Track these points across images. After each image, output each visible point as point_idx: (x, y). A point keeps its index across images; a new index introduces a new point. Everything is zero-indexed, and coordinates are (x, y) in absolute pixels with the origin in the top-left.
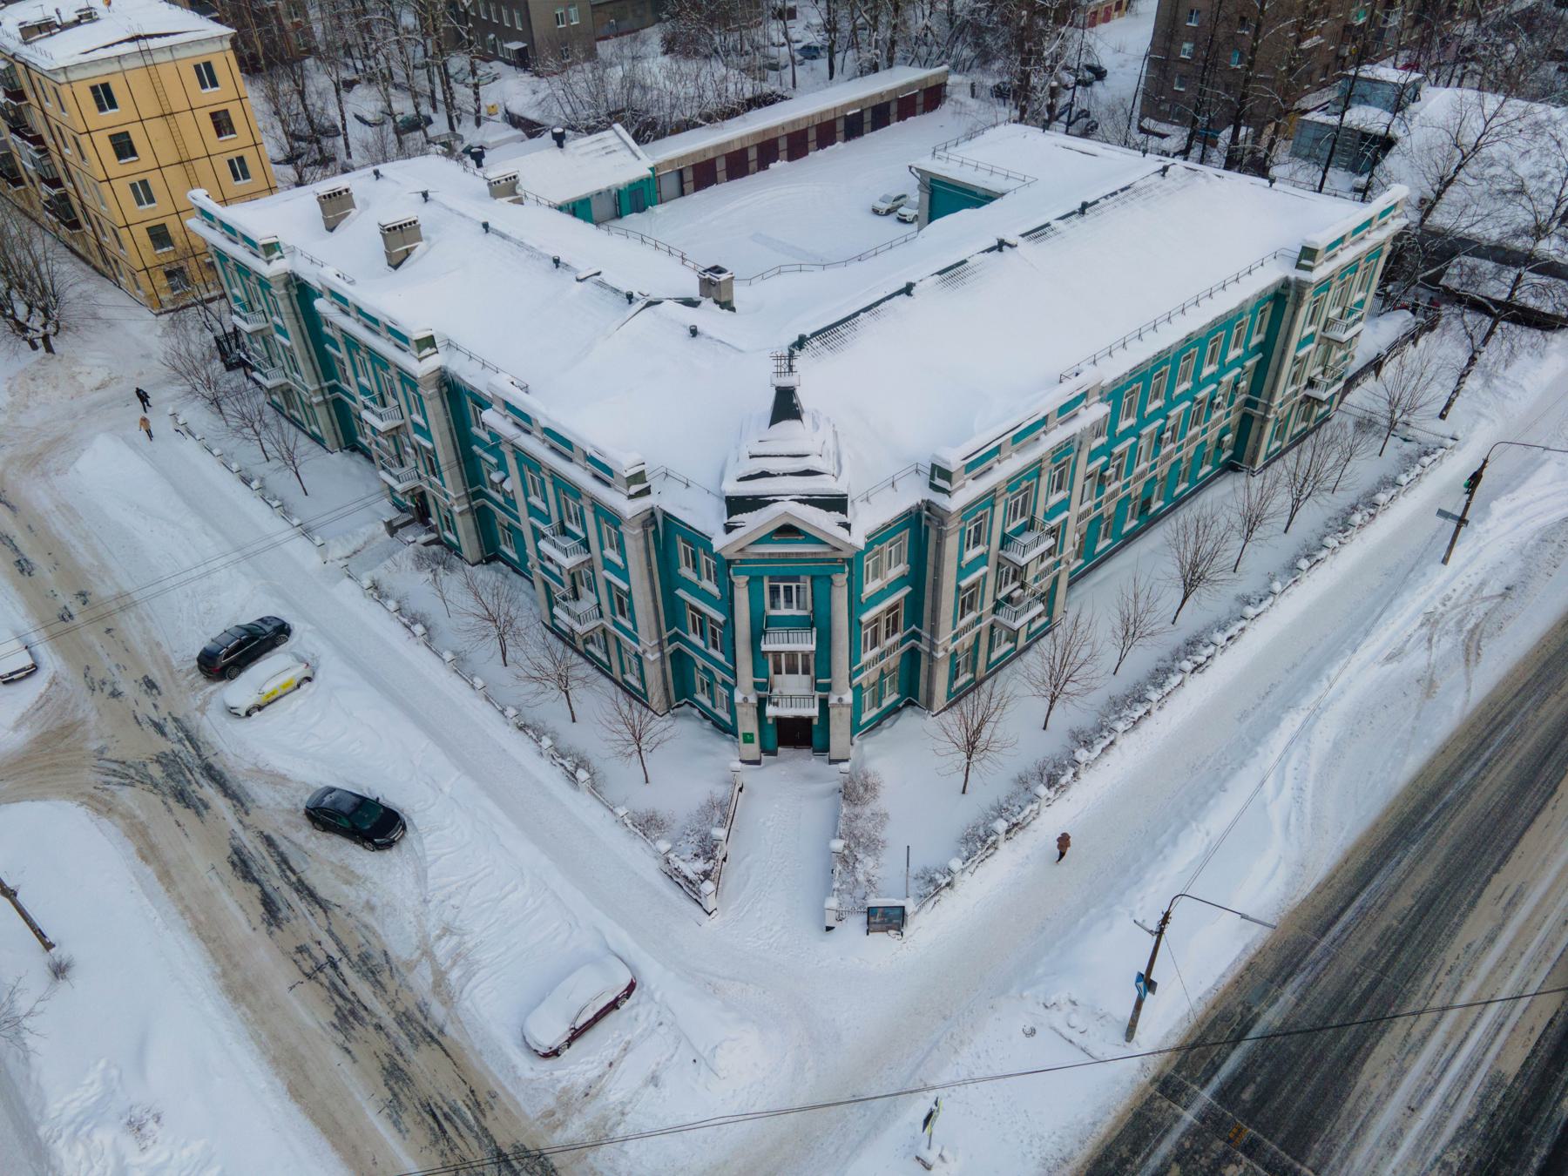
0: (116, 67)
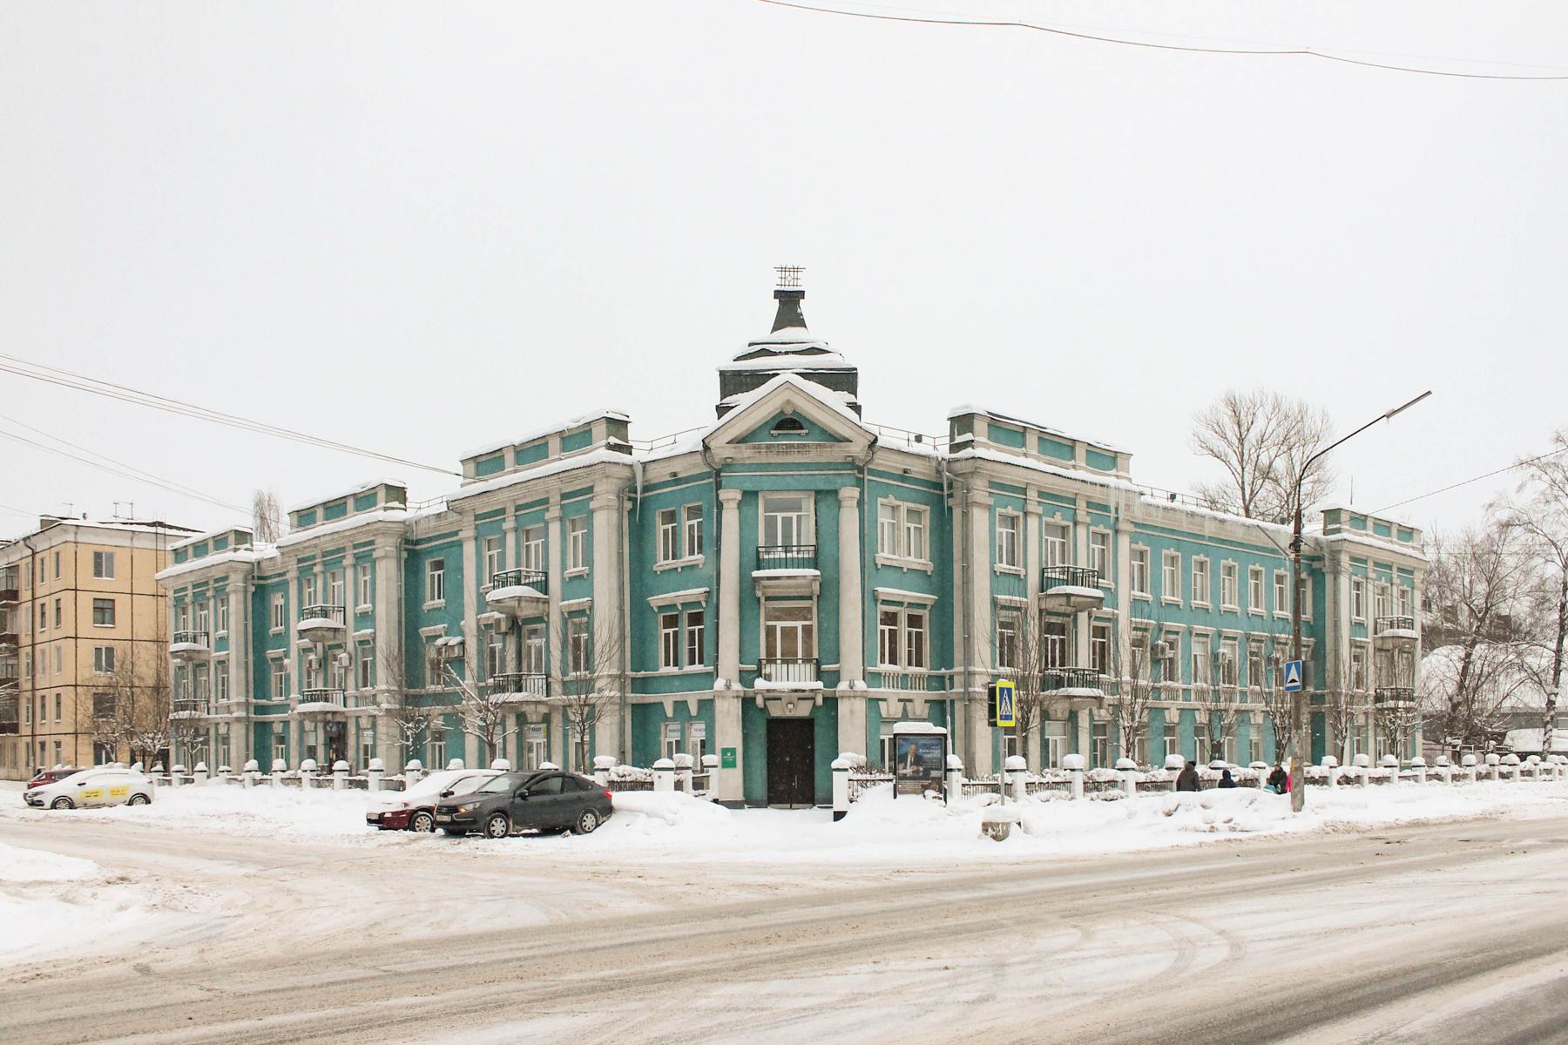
0: (127, 543)
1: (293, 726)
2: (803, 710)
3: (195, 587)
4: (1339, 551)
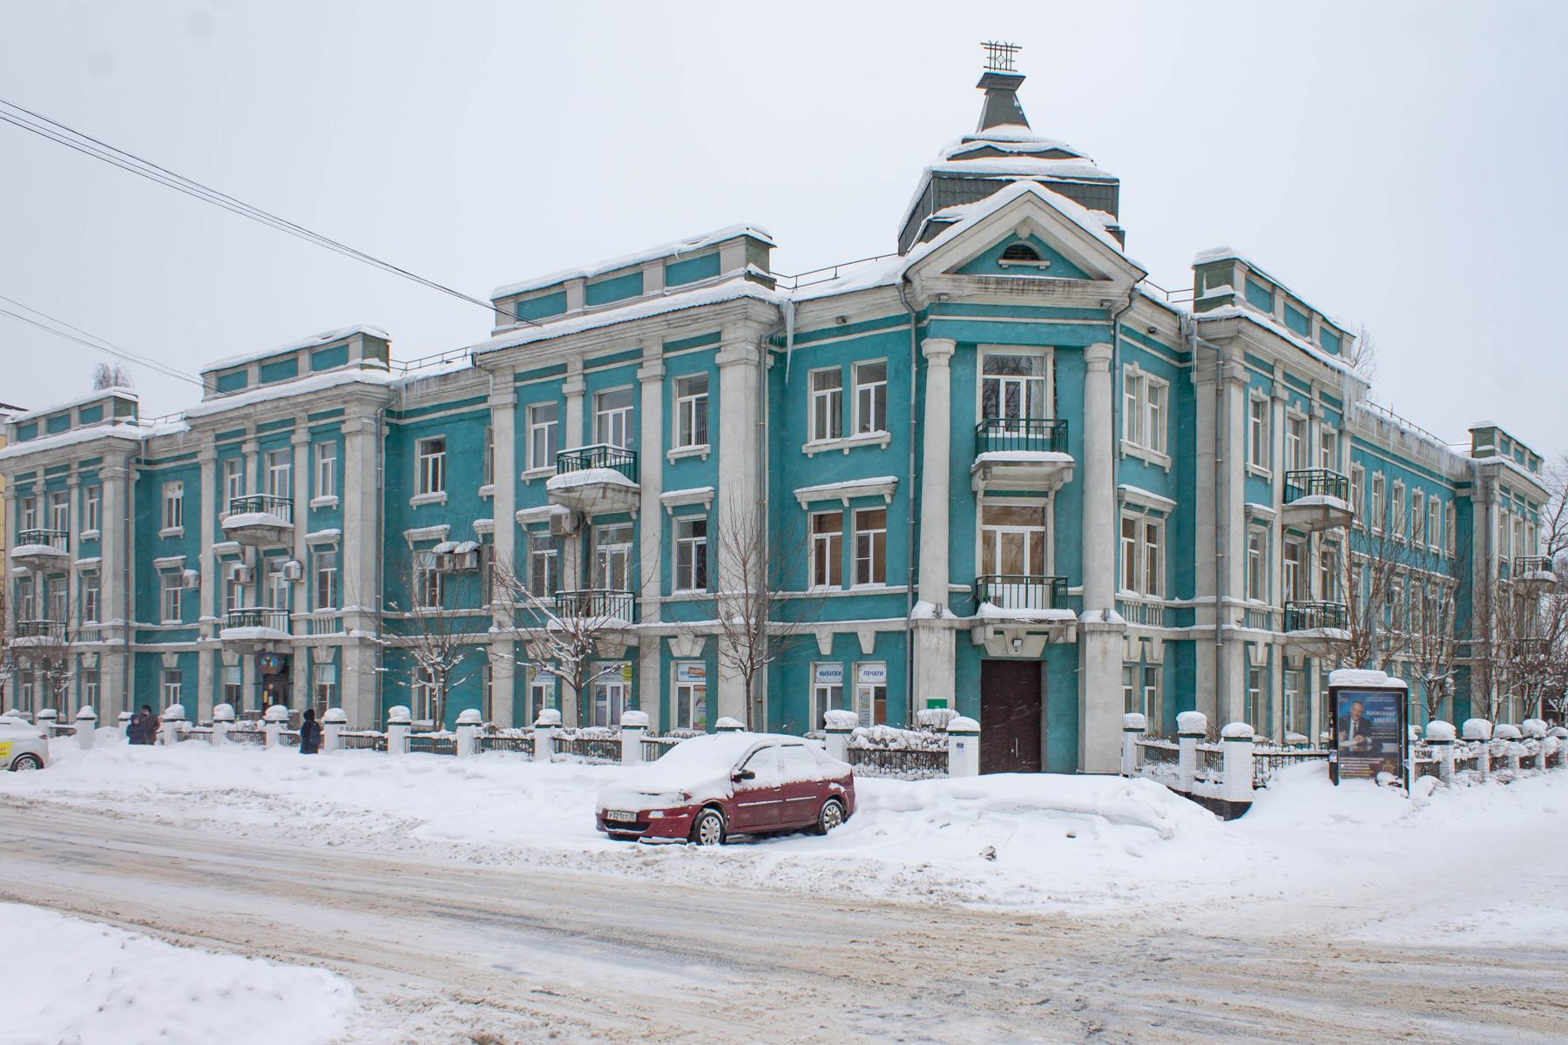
1: (205, 659)
2: (1032, 649)
3: (47, 472)
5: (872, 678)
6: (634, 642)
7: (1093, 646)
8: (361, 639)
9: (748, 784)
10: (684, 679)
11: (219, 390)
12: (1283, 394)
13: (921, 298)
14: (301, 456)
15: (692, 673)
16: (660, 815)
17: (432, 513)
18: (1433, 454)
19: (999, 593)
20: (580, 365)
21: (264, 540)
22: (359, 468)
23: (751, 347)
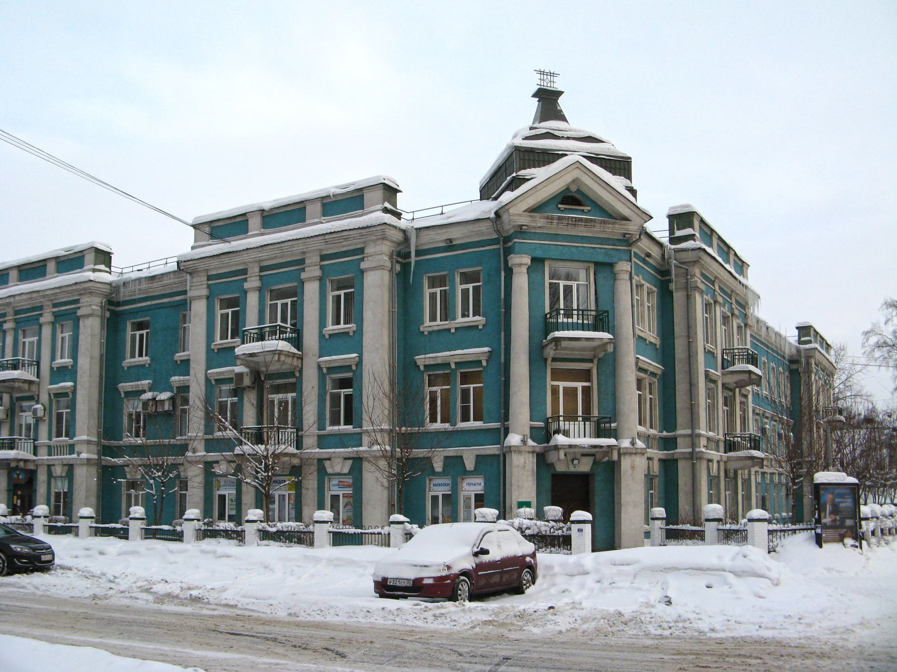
2: (584, 466)
4: (811, 357)
5: (472, 488)
6: (296, 461)
7: (626, 463)
8: (87, 459)
9: (485, 558)
10: (334, 489)
11: (324, 214)
12: (720, 299)
13: (507, 227)
14: (47, 331)
15: (341, 485)
16: (431, 581)
17: (138, 372)
18: (782, 343)
19: (567, 427)
20: (257, 270)
21: (20, 390)
22: (89, 339)
23: (386, 258)
